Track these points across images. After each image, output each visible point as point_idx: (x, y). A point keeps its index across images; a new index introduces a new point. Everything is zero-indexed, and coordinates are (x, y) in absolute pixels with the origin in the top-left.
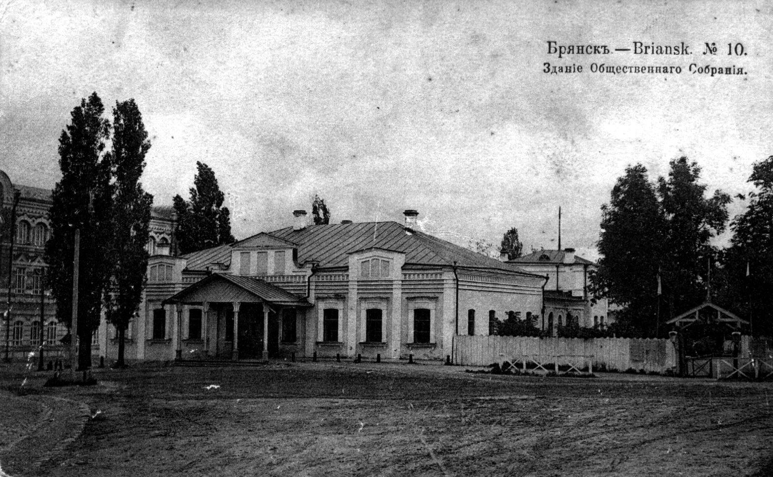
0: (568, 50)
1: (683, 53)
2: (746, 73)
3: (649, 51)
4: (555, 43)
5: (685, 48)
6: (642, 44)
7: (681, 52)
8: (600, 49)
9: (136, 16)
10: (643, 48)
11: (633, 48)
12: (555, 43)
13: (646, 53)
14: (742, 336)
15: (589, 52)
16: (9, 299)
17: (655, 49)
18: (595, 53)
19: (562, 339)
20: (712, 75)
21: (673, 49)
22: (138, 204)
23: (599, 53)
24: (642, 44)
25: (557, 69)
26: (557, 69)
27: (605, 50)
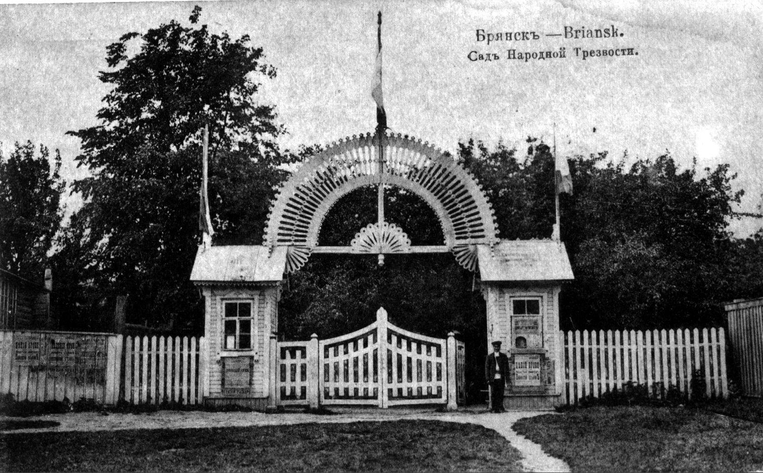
0: (496, 37)
1: (613, 36)
2: (637, 54)
3: (580, 35)
4: (483, 31)
5: (615, 30)
6: (572, 28)
7: (611, 35)
8: (528, 36)
9: (281, 70)
10: (574, 32)
11: (563, 32)
12: (483, 31)
13: (576, 37)
14: (501, 351)
15: (518, 38)
16: (217, 146)
17: (585, 34)
18: (523, 39)
19: (265, 395)
20: (584, 59)
21: (603, 33)
22: (30, 202)
23: (528, 39)
24: (572, 28)
25: (544, 55)
26: (544, 55)
27: (534, 36)
